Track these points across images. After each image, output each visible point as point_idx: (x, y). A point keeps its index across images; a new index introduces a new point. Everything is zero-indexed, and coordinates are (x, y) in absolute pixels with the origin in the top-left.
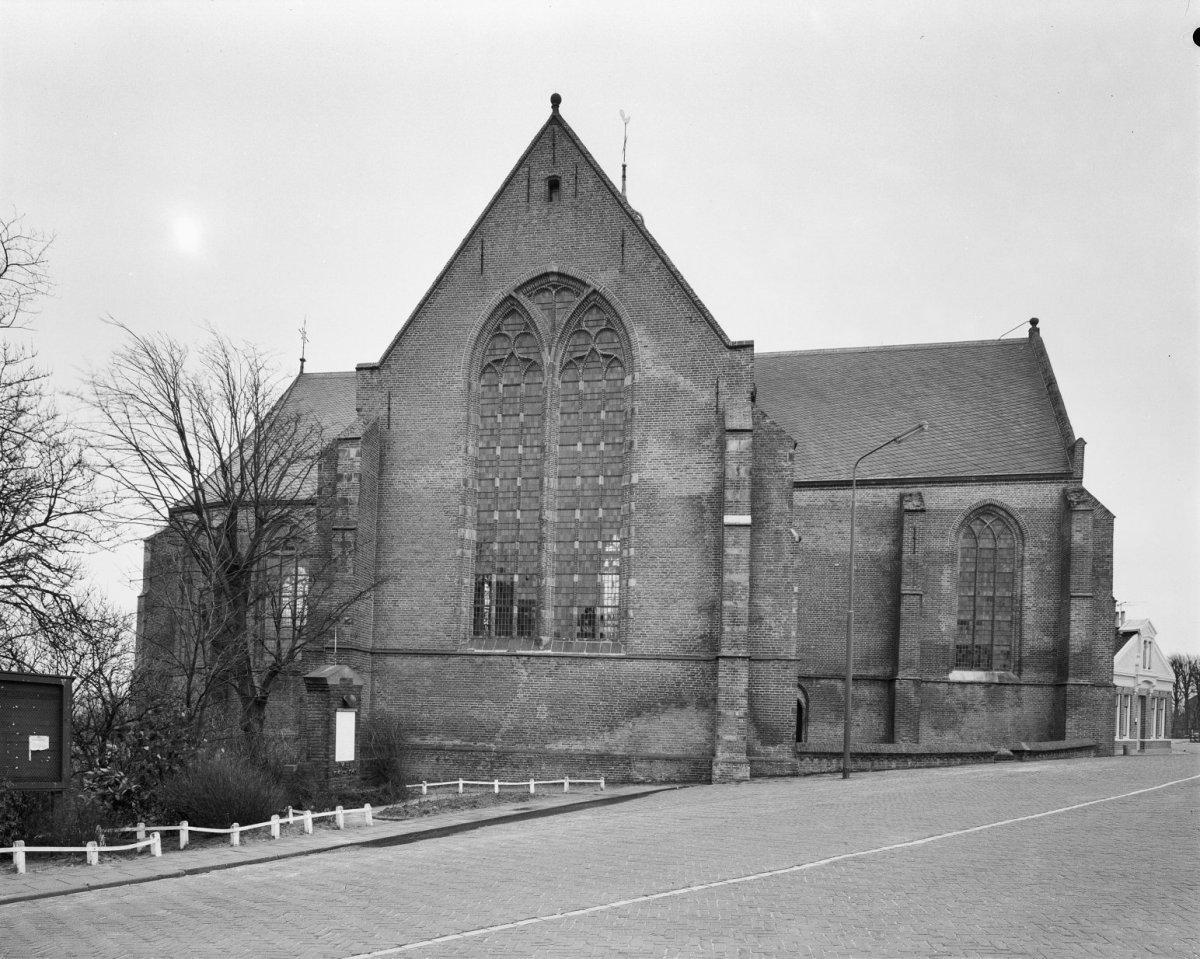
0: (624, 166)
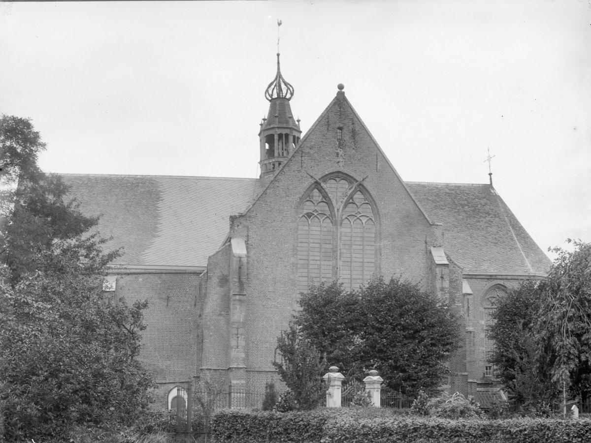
0: (278, 55)
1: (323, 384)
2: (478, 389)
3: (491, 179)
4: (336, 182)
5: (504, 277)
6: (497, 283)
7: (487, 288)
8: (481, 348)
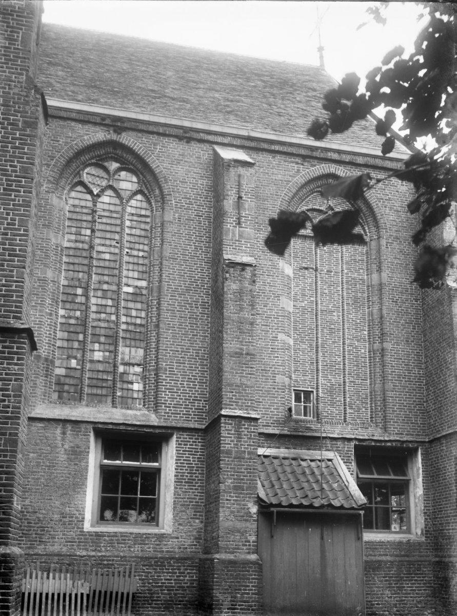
1: (217, 519)
2: (261, 451)
3: (321, 57)
4: (106, 176)
5: (347, 158)
6: (327, 171)
7: (300, 180)
8: (281, 336)
